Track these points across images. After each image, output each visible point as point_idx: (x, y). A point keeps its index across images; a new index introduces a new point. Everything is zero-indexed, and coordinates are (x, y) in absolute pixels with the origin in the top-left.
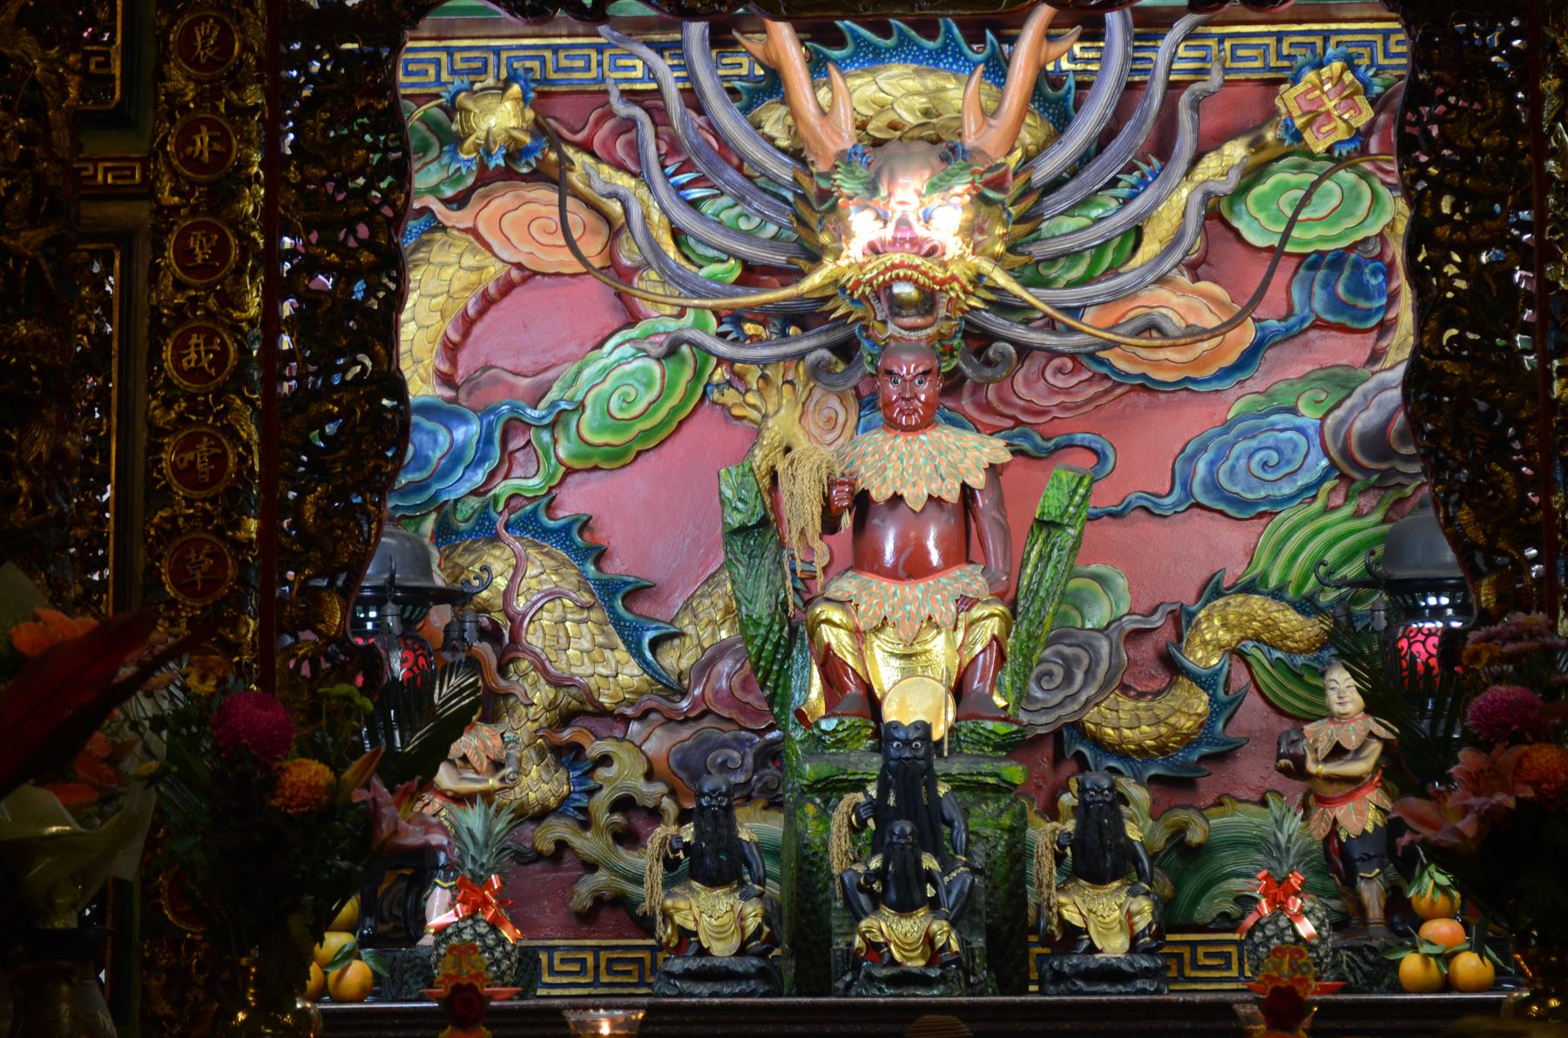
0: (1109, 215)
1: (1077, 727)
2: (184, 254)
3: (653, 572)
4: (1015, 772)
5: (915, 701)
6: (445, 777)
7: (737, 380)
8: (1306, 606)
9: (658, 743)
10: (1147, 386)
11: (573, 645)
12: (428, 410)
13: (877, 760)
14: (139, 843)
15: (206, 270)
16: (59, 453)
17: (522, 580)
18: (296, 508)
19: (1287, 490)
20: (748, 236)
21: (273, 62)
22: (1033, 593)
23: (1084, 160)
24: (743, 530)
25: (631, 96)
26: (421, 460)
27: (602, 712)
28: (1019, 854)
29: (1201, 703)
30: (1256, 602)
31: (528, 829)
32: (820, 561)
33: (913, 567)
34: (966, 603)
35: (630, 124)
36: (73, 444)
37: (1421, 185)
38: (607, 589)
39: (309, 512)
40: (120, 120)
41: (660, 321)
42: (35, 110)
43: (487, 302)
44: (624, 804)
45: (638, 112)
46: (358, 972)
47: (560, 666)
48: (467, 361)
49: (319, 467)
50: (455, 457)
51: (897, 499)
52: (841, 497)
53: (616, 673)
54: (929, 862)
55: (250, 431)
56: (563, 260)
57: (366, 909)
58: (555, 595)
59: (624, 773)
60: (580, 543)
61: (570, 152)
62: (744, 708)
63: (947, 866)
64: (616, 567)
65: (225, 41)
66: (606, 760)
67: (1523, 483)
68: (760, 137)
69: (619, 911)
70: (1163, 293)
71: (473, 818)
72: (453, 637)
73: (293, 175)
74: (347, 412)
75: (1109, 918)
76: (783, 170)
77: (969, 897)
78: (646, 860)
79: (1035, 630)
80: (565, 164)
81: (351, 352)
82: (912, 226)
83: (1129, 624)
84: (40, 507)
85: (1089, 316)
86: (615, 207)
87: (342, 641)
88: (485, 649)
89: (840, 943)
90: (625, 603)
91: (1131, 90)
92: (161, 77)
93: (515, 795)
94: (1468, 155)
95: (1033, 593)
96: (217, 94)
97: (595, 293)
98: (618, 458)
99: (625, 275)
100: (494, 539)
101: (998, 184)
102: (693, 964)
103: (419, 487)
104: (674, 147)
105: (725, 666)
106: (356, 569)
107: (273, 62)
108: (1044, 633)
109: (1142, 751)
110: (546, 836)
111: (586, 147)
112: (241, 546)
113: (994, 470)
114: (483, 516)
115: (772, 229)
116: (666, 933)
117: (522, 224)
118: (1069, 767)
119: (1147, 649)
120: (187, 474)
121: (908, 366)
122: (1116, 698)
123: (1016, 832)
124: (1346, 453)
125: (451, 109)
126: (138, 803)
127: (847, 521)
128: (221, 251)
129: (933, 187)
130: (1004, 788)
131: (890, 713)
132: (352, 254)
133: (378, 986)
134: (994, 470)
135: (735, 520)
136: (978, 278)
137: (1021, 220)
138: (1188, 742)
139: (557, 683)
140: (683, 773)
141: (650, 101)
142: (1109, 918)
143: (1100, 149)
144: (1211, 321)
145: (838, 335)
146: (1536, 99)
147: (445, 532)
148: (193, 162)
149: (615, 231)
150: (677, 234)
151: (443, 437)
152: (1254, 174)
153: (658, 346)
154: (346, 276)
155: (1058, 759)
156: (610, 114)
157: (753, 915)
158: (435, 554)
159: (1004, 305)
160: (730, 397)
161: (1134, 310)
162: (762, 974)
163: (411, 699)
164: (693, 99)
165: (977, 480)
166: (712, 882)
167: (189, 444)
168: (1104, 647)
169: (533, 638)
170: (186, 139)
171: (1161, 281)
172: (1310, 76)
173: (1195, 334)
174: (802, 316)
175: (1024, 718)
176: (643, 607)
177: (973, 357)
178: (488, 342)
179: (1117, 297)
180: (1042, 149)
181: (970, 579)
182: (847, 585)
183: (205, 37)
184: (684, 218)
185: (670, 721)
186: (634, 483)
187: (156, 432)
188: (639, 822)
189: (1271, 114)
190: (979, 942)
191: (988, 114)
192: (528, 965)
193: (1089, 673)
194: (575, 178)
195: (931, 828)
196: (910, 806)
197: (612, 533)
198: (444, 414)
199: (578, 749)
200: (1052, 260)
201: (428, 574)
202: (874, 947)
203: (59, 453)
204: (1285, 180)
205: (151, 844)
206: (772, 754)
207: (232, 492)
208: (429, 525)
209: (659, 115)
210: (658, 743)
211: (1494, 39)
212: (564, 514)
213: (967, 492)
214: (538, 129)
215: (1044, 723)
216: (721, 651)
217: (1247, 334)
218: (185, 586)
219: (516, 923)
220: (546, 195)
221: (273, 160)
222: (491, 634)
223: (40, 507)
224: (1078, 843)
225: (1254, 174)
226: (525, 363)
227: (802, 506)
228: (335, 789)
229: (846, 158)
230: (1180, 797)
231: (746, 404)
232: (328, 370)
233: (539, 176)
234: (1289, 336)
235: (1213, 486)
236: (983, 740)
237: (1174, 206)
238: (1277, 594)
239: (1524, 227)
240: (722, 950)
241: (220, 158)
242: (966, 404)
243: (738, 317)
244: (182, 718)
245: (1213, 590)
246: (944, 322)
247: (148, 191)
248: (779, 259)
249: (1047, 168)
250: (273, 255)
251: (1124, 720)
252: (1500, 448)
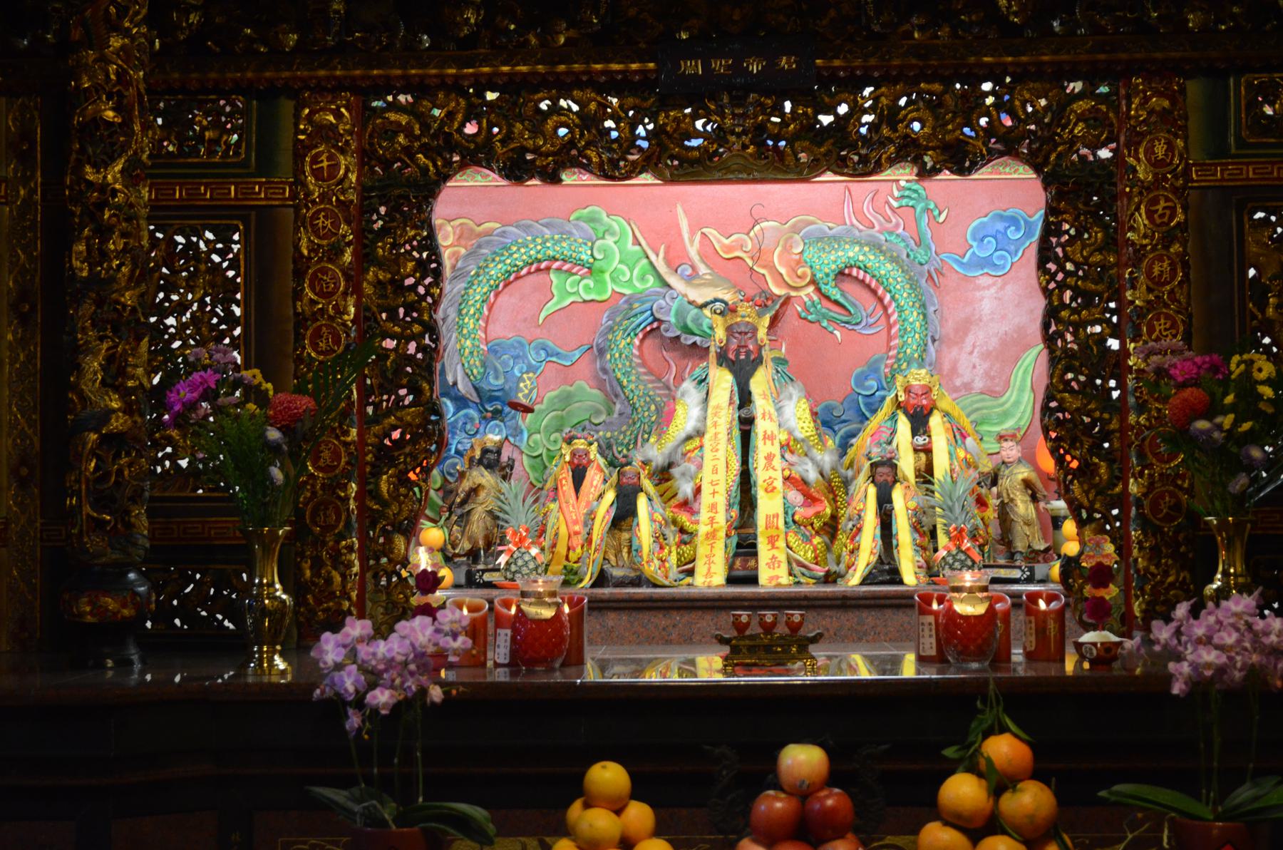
37: (1052, 285)
112: (346, 444)
239: (1113, 312)
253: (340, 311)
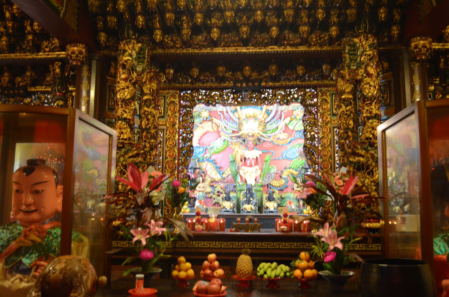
0: (274, 126)
1: (270, 184)
2: (170, 132)
3: (223, 165)
4: (262, 189)
5: (251, 181)
6: (197, 188)
7: (232, 144)
8: (296, 170)
9: (222, 185)
10: (278, 145)
11: (212, 173)
12: (197, 147)
13: (246, 188)
14: (164, 196)
15: (172, 133)
16: (156, 154)
17: (208, 167)
18: (181, 160)
19: (294, 157)
20: (233, 128)
21: (179, 111)
22: (264, 169)
23: (271, 119)
24: (232, 161)
25: (220, 112)
26: (196, 153)
27: (216, 181)
28: (262, 199)
29: (284, 181)
30: (291, 170)
31: (208, 194)
32: (240, 165)
33: (251, 166)
34: (257, 170)
35: (220, 115)
36: (157, 153)
38: (217, 167)
39: (183, 160)
40: (163, 117)
41: (223, 138)
42: (154, 117)
43: (204, 135)
44: (218, 192)
45: (221, 114)
46: (188, 210)
47: (211, 176)
48: (201, 142)
49: (184, 155)
50: (200, 152)
51: (249, 158)
52: (243, 158)
53: (217, 177)
54: (251, 199)
55: (176, 151)
56: (212, 130)
57: (189, 203)
58: (211, 168)
59: (218, 189)
60: (214, 162)
61: (213, 118)
62: (232, 181)
63: (253, 199)
64: (218, 165)
65: (174, 108)
66: (216, 187)
67: (316, 158)
68: (235, 117)
69: (217, 204)
70: (280, 134)
71: (201, 193)
72: (199, 173)
73: (181, 123)
74: (187, 149)
75: (272, 206)
76: (237, 120)
77: (256, 203)
78: (220, 198)
79: (265, 173)
80: (212, 119)
81: (188, 142)
82: (251, 128)
83: (276, 172)
84: (154, 160)
85: (272, 137)
86: (218, 124)
87: (186, 174)
88: (203, 174)
89: (241, 208)
90: (219, 169)
91: (277, 111)
92: (167, 112)
93: (206, 191)
94: (310, 122)
95: (264, 169)
96: (173, 114)
97: (216, 135)
98: (219, 153)
99: (219, 132)
100: (204, 162)
101: (261, 122)
102: (225, 210)
103: (196, 156)
104: (225, 117)
105: (230, 177)
106: (188, 166)
107: (179, 111)
108: (266, 173)
109: (277, 187)
110: (209, 195)
111: (215, 117)
112: (175, 164)
113: (260, 155)
114: (203, 159)
115: (236, 127)
116: (222, 207)
117: (208, 126)
118: (269, 188)
119: (278, 175)
120: (170, 156)
121: (250, 143)
122: (274, 180)
123: (262, 196)
124: (301, 153)
125: (200, 113)
126: (164, 192)
127: (243, 160)
128: (173, 131)
129: (65, 273)
130: (260, 191)
131: (248, 183)
132: (187, 132)
133: (190, 212)
134: (260, 155)
135: (231, 160)
136: (259, 133)
137: (264, 126)
138: (283, 186)
139: (211, 178)
140: (225, 188)
141: (222, 112)
142: (272, 206)
143: (270, 121)
144: (286, 138)
145: (243, 139)
146: (317, 116)
147: (198, 161)
148: (171, 122)
149: (218, 127)
150: (225, 127)
151: (198, 150)
152: (291, 121)
153: (223, 140)
154: (187, 134)
155: (268, 187)
156: (217, 114)
157: (232, 205)
158: (197, 163)
159: (262, 136)
160: (231, 146)
161: (277, 137)
162: (233, 211)
163: (194, 180)
164: (227, 112)
165: (258, 156)
166: (227, 201)
167: (170, 152)
168: (273, 175)
169: (208, 173)
170: (170, 119)
171: (280, 133)
172: (297, 110)
173: (283, 140)
174: (239, 137)
175: (263, 182)
176: (221, 169)
177: (258, 142)
178: (204, 139)
179: (275, 135)
180: (267, 118)
181: (257, 167)
182: (244, 168)
183: (172, 108)
184: (226, 126)
185: (224, 182)
186: (220, 156)
187: (166, 151)
188: (220, 194)
189: (293, 114)
190: (257, 208)
191: (260, 114)
192: (207, 210)
193: (271, 178)
194: (214, 121)
195: (252, 195)
196: (249, 193)
197: (218, 161)
198: (198, 147)
199: (213, 186)
200: (268, 131)
201: (196, 165)
202: (245, 209)
203: (156, 154)
204: (294, 122)
205: (165, 196)
206: (235, 187)
207: (174, 158)
208: (197, 160)
209: (223, 114)
210: (222, 185)
211: (313, 109)
212: (212, 159)
213: (257, 158)
214: (210, 115)
215: (266, 183)
216: (229, 175)
217: (290, 139)
218: (169, 168)
219: (205, 205)
220: (210, 123)
221: (179, 122)
222: (204, 172)
223: (154, 160)
224: (269, 197)
225: (291, 121)
226: (208, 142)
227: (238, 159)
228: (185, 191)
229: (244, 119)
230: (282, 192)
231: (233, 147)
232: (185, 144)
233: (210, 121)
234: (295, 140)
235: (286, 156)
236: (258, 185)
237: (282, 124)
238: (293, 169)
240: (228, 209)
241: (173, 121)
242: (258, 147)
243: (232, 137)
244: (169, 183)
245: (285, 168)
246: (255, 138)
247: (166, 125)
248: (237, 130)
249: (267, 121)
250: (179, 132)
251: (275, 183)
252: (313, 154)
253: (174, 137)
